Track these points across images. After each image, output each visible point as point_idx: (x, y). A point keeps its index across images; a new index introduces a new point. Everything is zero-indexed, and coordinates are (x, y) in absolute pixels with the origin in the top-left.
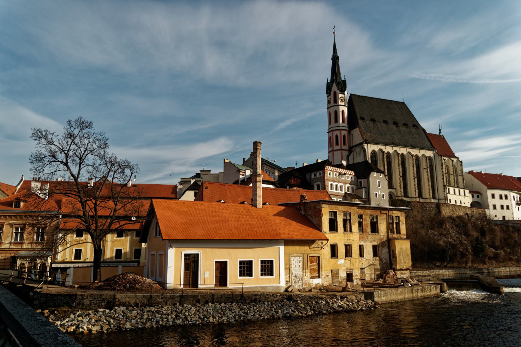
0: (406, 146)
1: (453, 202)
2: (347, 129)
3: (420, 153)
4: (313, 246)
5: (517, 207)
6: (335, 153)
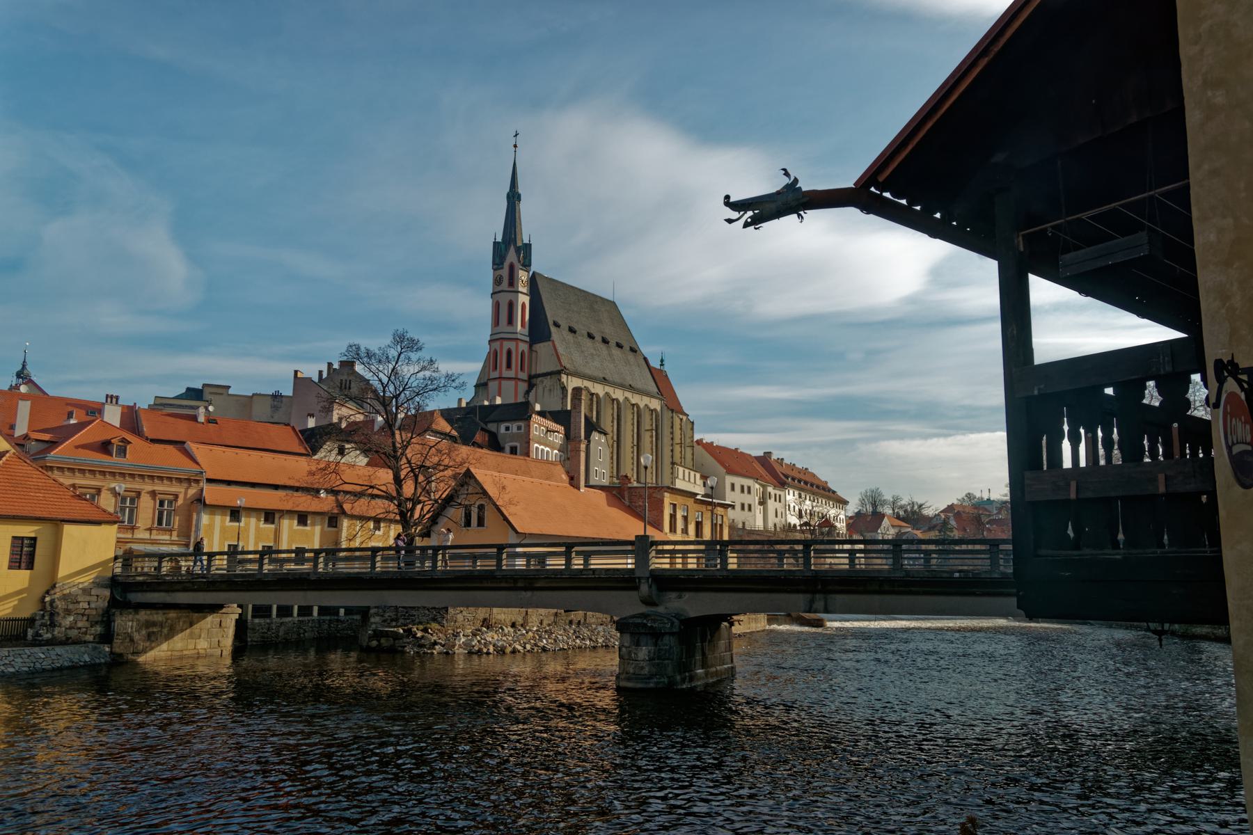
0: (622, 386)
3: (642, 401)
6: (503, 382)
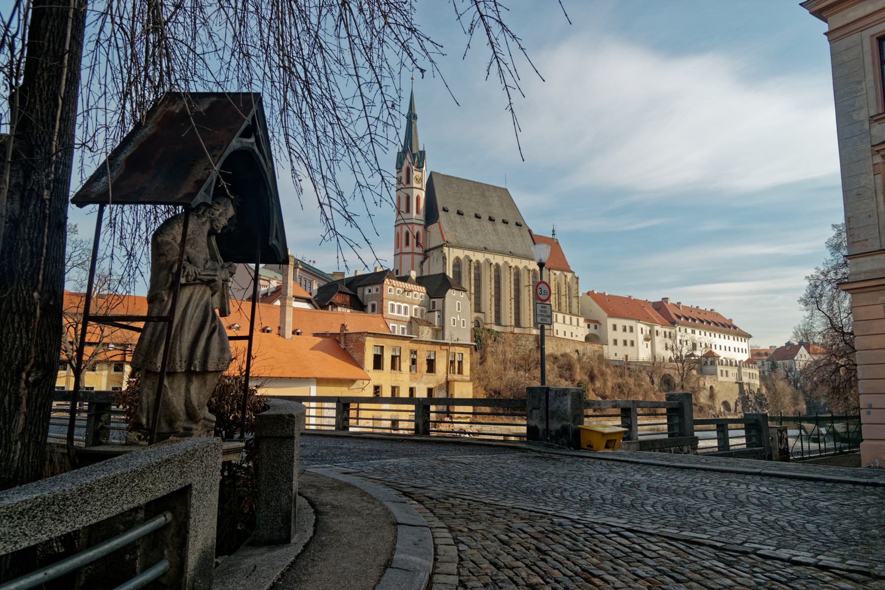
0: (502, 253)
1: (561, 335)
2: (422, 223)
4: (352, 387)
5: (645, 343)
6: (404, 256)
